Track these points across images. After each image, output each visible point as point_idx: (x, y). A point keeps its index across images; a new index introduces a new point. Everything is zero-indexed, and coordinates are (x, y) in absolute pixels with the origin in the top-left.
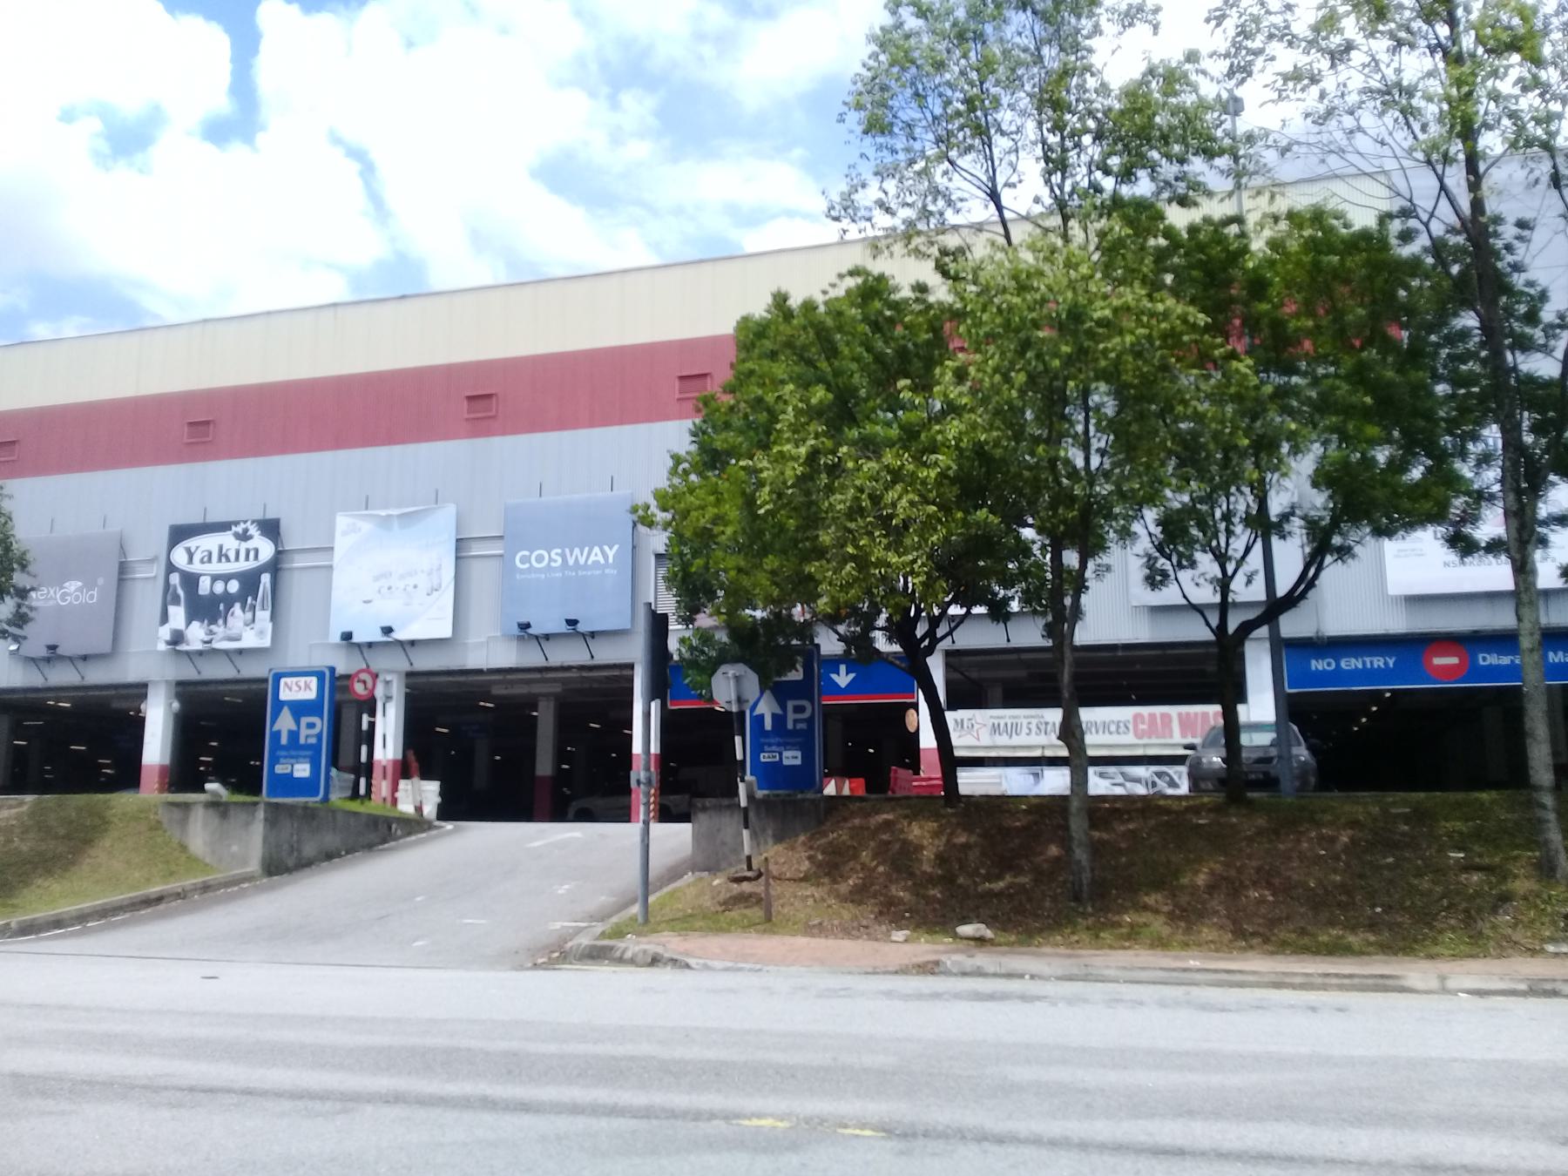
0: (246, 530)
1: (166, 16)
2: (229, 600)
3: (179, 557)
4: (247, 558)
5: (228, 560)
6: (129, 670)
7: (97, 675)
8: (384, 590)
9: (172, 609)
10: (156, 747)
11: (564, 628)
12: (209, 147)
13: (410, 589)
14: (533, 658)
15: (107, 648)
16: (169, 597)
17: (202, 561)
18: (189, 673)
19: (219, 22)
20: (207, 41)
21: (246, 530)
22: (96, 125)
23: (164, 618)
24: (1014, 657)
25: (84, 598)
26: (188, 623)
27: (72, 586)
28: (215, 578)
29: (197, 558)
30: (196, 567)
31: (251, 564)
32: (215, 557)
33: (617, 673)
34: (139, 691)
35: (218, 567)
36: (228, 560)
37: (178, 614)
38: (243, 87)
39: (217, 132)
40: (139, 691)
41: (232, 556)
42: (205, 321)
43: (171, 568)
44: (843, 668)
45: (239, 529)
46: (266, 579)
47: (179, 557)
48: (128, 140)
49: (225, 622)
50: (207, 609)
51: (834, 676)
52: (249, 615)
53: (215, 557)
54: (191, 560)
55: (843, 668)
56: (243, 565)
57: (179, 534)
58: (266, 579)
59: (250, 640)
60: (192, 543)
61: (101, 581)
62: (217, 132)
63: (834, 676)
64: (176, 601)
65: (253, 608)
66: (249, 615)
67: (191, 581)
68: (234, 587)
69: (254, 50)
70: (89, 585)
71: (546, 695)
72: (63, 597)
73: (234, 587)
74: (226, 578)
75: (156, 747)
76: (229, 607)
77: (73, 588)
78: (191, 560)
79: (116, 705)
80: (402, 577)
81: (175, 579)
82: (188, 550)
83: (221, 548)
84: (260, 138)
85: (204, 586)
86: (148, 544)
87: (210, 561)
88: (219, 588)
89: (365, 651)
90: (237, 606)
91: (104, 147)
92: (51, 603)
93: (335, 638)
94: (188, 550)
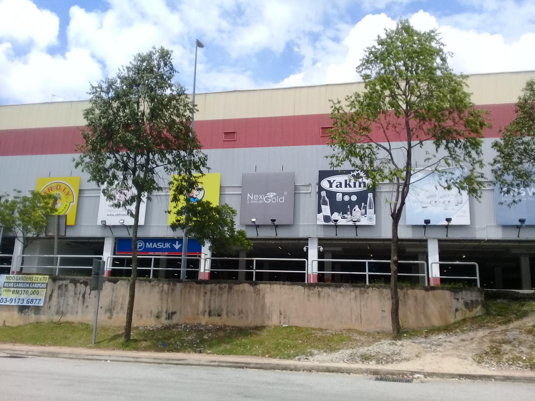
0: (358, 174)
1: (38, 10)
2: (352, 204)
3: (325, 184)
4: (360, 186)
5: (350, 186)
6: (302, 234)
7: (283, 234)
8: (433, 203)
9: (323, 207)
10: (312, 268)
11: (270, 223)
12: (49, 57)
13: (447, 202)
14: (512, 235)
15: (292, 223)
16: (320, 202)
17: (337, 186)
18: (331, 234)
19: (55, 13)
20: (49, 21)
21: (358, 174)
22: (9, 45)
23: (320, 211)
24: (329, 242)
25: (278, 200)
26: (332, 214)
27: (271, 195)
28: (344, 194)
29: (334, 185)
30: (334, 189)
31: (362, 189)
32: (343, 185)
33: (87, 241)
34: (306, 240)
35: (344, 189)
36: (350, 186)
37: (326, 210)
38: (63, 35)
39: (52, 51)
40: (306, 240)
41: (352, 184)
42: (327, 85)
43: (321, 189)
44: (177, 242)
45: (355, 173)
46: (370, 195)
47: (325, 184)
48: (20, 51)
49: (351, 214)
50: (336, 207)
51: (174, 245)
52: (363, 211)
53: (343, 185)
54: (331, 186)
55: (177, 242)
56: (358, 189)
57: (323, 175)
58: (370, 195)
59: (364, 221)
60: (332, 179)
61: (286, 193)
62: (52, 51)
63: (174, 245)
64: (325, 203)
65: (365, 208)
66: (363, 211)
67: (331, 195)
68: (354, 198)
69: (68, 24)
70: (280, 194)
71: (329, 251)
72: (267, 199)
73: (354, 198)
74: (350, 194)
75: (312, 268)
76: (352, 207)
77: (272, 196)
78: (331, 186)
79: (514, 251)
80: (441, 197)
81: (323, 194)
82: (329, 181)
83: (346, 181)
84: (67, 54)
85: (339, 197)
86: (308, 177)
87: (341, 186)
88: (347, 198)
89: (129, 228)
90: (357, 207)
91: (11, 52)
92: (261, 202)
93: (99, 223)
94: (329, 181)
